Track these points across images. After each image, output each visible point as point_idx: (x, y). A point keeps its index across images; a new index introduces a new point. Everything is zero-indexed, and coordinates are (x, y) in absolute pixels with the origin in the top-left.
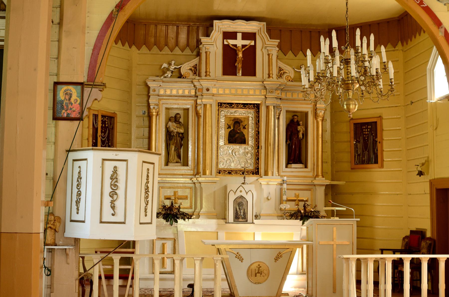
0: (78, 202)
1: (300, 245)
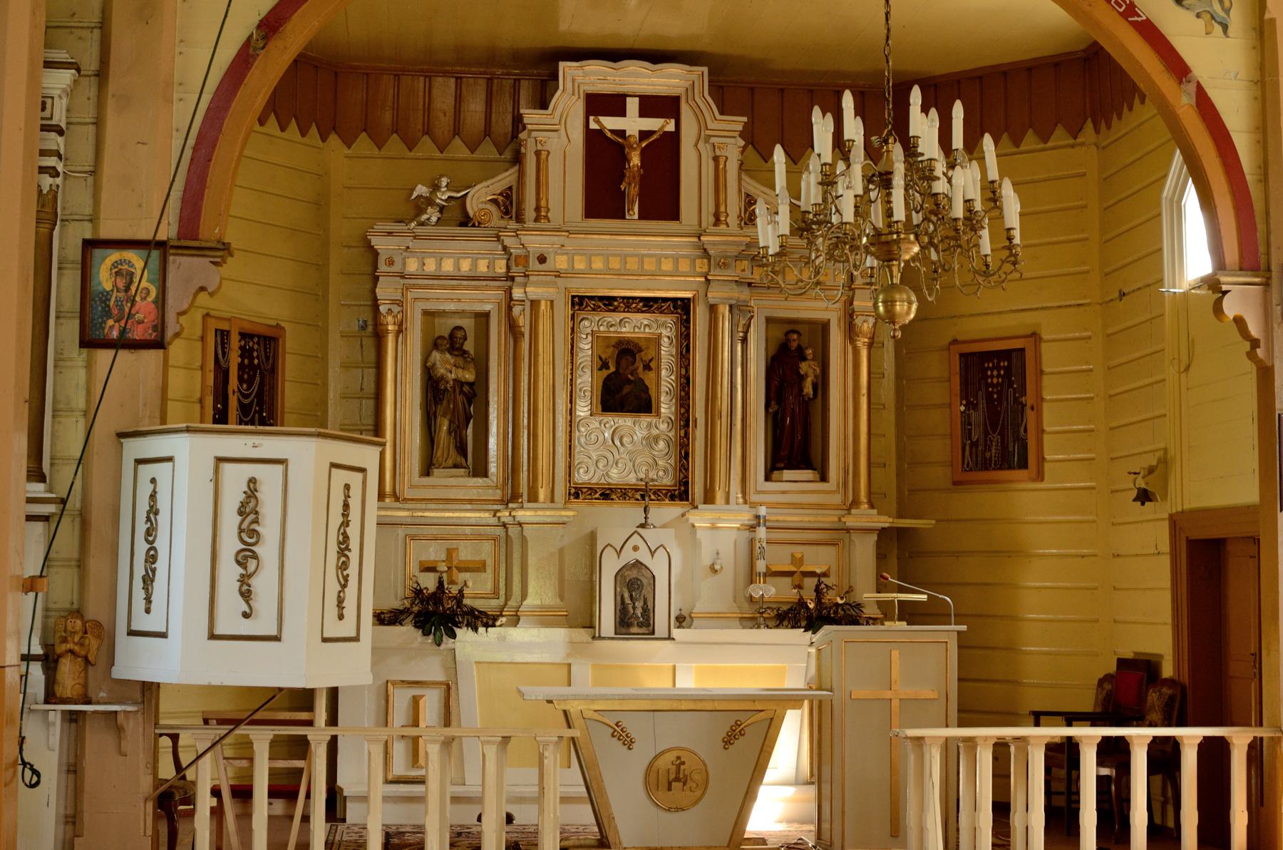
0: (148, 580)
1: (792, 700)
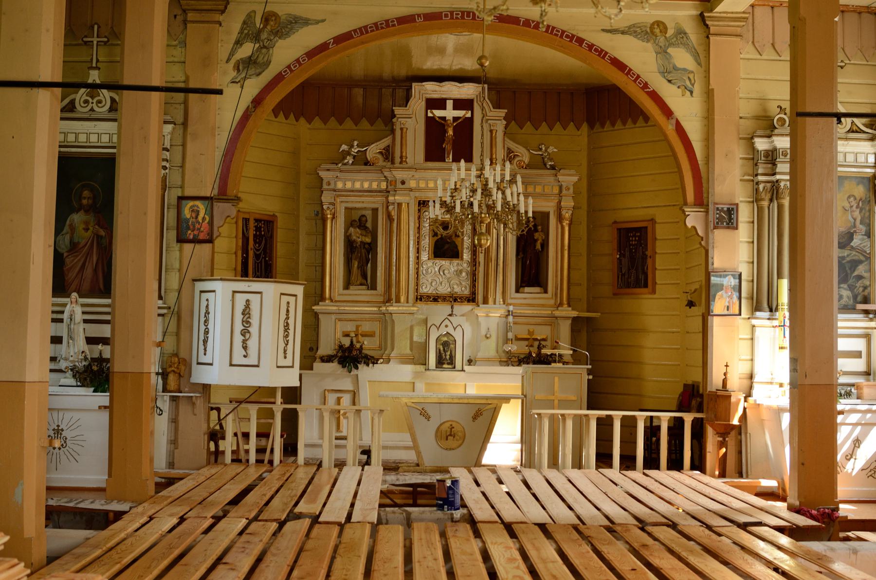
0: (205, 342)
